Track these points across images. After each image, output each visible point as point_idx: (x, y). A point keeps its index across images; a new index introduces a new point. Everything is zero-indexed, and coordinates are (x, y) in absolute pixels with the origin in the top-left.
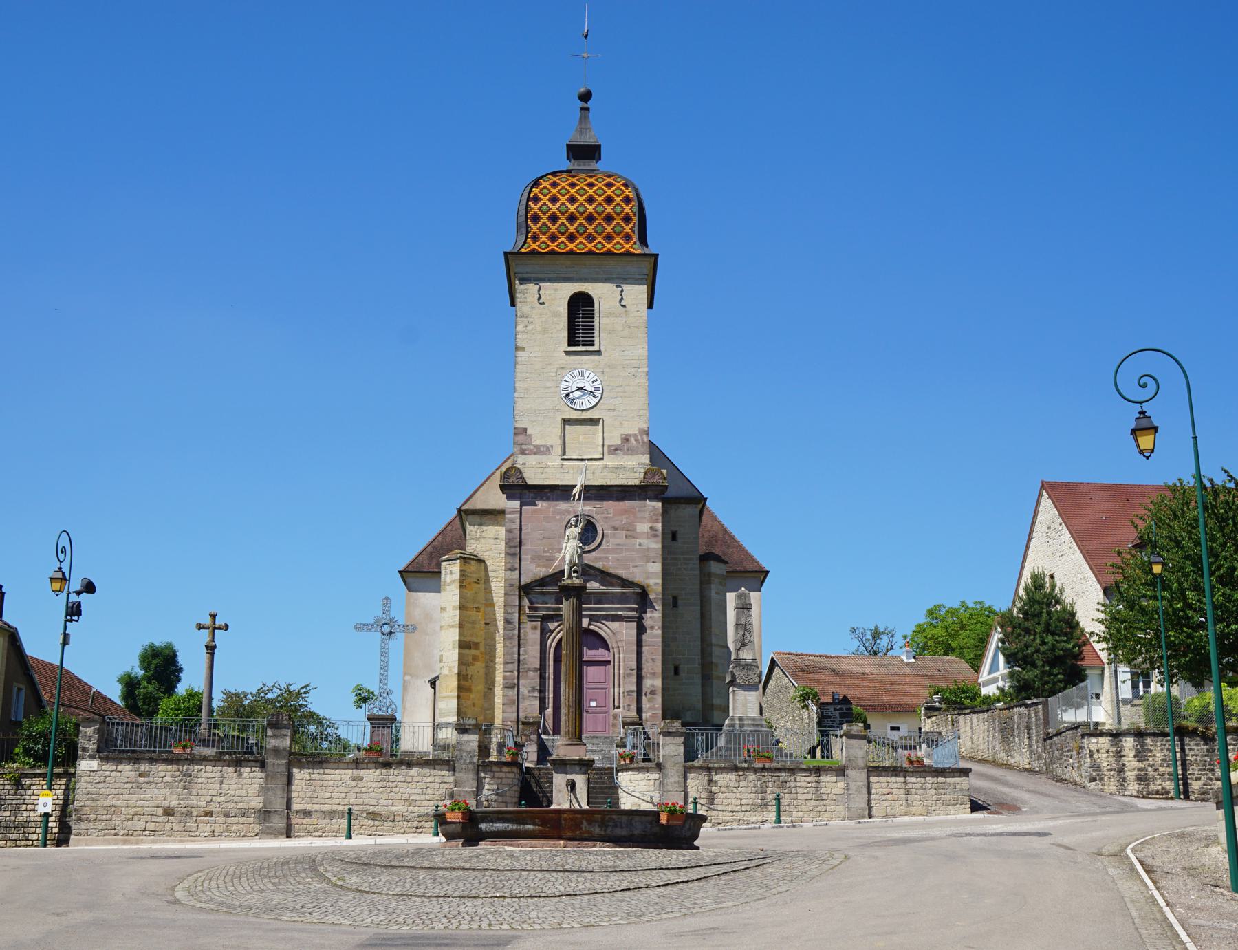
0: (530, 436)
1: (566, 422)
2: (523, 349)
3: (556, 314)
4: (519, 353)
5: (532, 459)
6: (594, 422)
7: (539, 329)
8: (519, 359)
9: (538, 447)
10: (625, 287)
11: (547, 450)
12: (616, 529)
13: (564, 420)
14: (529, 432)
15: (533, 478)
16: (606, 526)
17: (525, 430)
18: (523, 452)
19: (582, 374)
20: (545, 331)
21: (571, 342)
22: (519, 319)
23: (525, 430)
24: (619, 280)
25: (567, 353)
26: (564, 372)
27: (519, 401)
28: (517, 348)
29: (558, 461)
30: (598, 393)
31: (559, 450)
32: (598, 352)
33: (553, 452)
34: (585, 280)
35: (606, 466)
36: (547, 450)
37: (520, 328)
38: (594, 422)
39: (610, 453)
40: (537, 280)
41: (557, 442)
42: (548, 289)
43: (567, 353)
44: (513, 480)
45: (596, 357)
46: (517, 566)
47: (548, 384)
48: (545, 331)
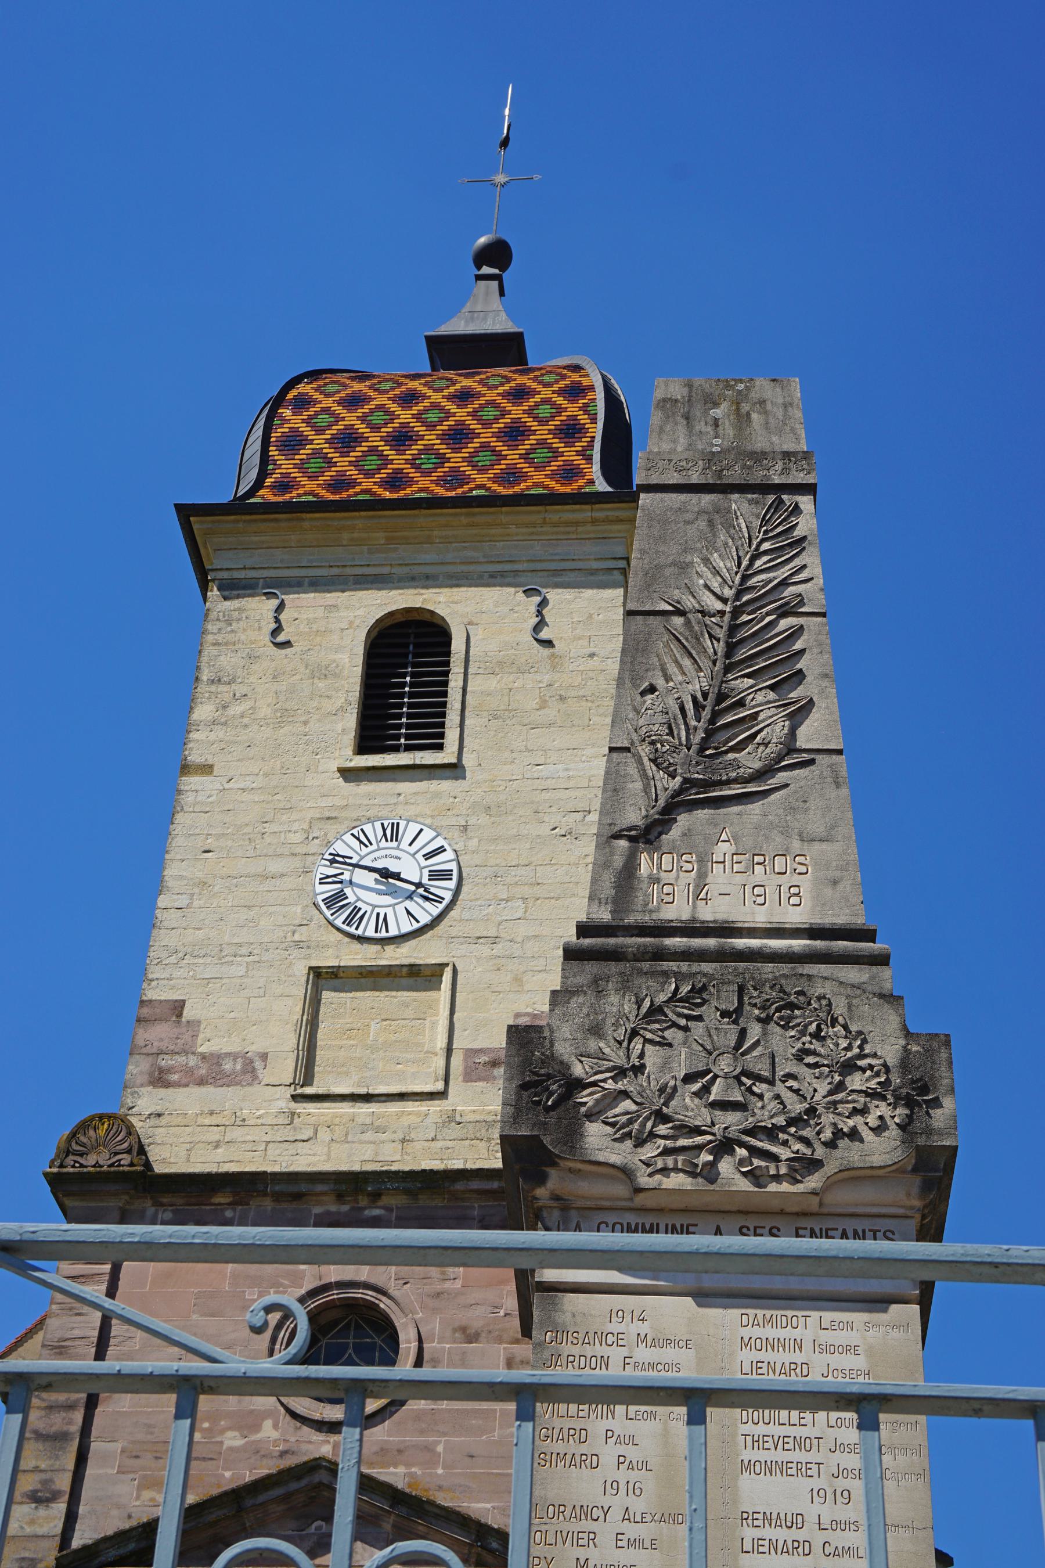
0: (194, 1025)
1: (323, 978)
2: (206, 769)
3: (324, 672)
4: (191, 782)
5: (186, 1100)
6: (421, 977)
7: (264, 711)
8: (188, 799)
9: (214, 1060)
10: (554, 595)
11: (249, 1069)
12: (472, 1338)
13: (316, 972)
14: (188, 1014)
15: (170, 1156)
16: (434, 1326)
17: (178, 1007)
18: (160, 1079)
19: (394, 834)
20: (283, 716)
21: (366, 744)
22: (202, 688)
23: (178, 1007)
24: (535, 578)
25: (348, 774)
26: (332, 829)
27: (167, 918)
28: (186, 769)
29: (281, 1100)
30: (444, 889)
31: (285, 1068)
32: (455, 770)
33: (266, 1076)
34: (428, 581)
35: (451, 1118)
36: (249, 1069)
37: (202, 712)
38: (421, 977)
39: (470, 1076)
40: (275, 586)
41: (282, 1043)
42: (305, 609)
43: (348, 774)
44: (98, 1160)
45: (445, 786)
46: (64, 1483)
47: (275, 866)
48: (283, 716)
